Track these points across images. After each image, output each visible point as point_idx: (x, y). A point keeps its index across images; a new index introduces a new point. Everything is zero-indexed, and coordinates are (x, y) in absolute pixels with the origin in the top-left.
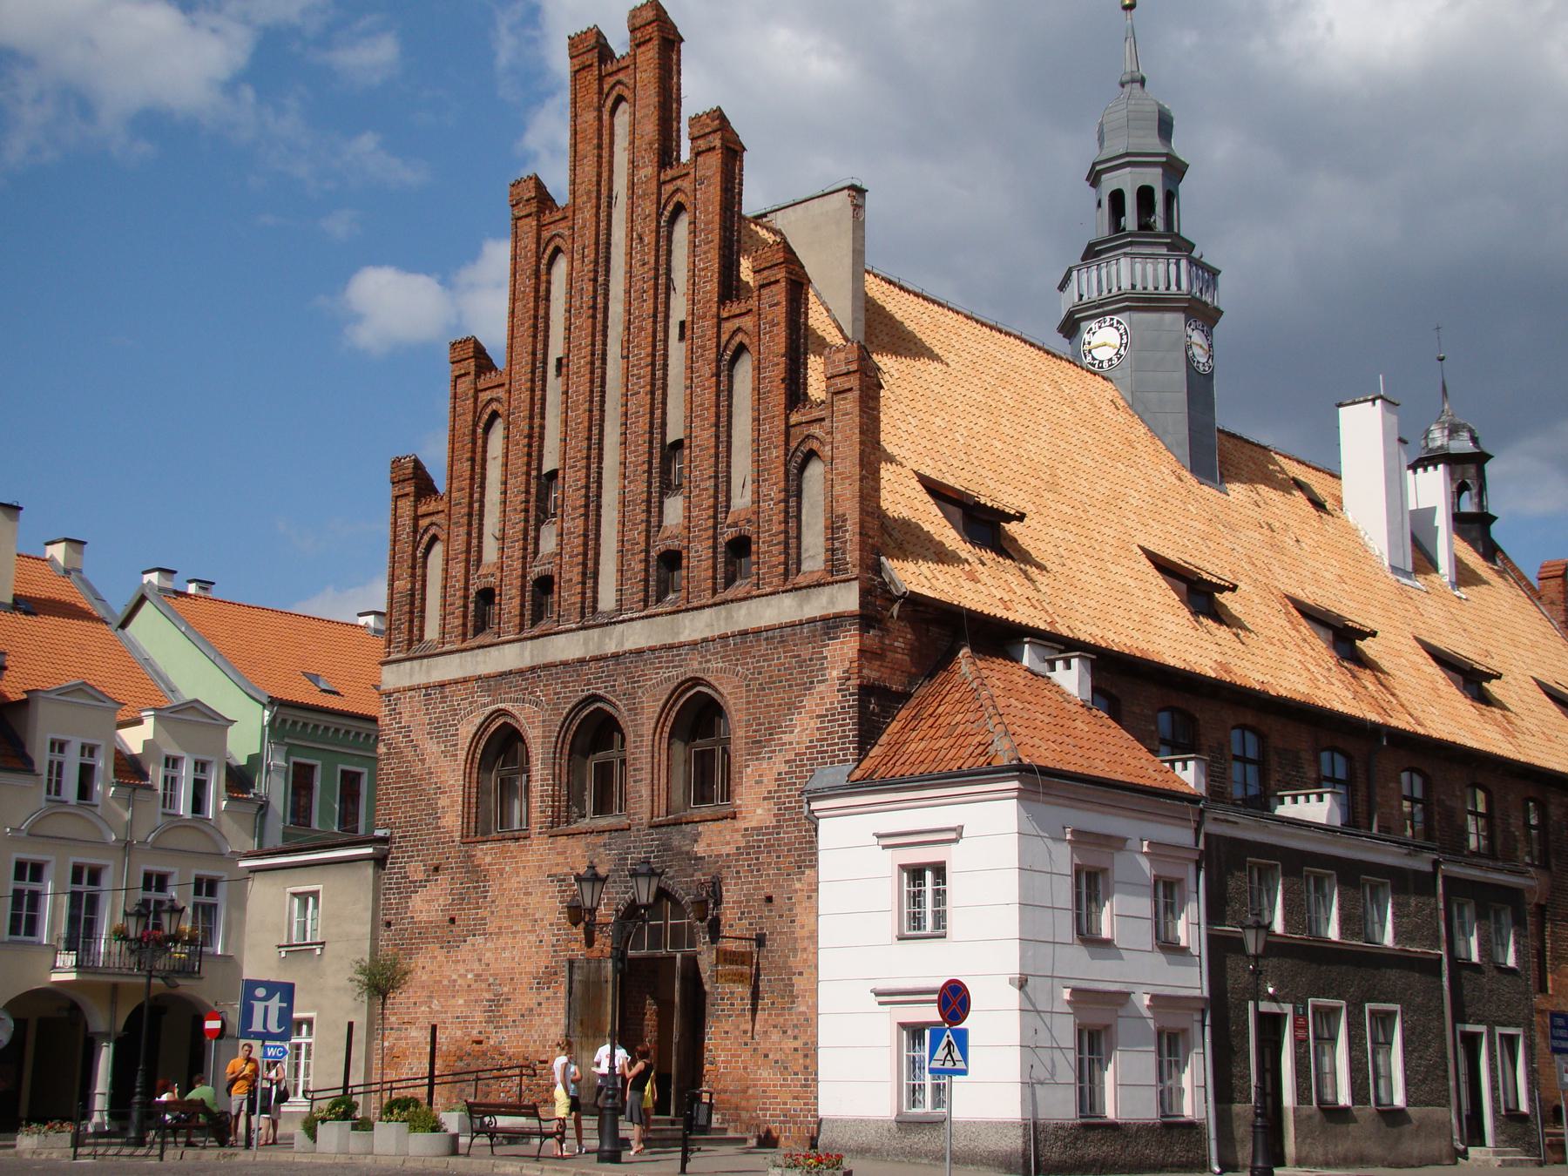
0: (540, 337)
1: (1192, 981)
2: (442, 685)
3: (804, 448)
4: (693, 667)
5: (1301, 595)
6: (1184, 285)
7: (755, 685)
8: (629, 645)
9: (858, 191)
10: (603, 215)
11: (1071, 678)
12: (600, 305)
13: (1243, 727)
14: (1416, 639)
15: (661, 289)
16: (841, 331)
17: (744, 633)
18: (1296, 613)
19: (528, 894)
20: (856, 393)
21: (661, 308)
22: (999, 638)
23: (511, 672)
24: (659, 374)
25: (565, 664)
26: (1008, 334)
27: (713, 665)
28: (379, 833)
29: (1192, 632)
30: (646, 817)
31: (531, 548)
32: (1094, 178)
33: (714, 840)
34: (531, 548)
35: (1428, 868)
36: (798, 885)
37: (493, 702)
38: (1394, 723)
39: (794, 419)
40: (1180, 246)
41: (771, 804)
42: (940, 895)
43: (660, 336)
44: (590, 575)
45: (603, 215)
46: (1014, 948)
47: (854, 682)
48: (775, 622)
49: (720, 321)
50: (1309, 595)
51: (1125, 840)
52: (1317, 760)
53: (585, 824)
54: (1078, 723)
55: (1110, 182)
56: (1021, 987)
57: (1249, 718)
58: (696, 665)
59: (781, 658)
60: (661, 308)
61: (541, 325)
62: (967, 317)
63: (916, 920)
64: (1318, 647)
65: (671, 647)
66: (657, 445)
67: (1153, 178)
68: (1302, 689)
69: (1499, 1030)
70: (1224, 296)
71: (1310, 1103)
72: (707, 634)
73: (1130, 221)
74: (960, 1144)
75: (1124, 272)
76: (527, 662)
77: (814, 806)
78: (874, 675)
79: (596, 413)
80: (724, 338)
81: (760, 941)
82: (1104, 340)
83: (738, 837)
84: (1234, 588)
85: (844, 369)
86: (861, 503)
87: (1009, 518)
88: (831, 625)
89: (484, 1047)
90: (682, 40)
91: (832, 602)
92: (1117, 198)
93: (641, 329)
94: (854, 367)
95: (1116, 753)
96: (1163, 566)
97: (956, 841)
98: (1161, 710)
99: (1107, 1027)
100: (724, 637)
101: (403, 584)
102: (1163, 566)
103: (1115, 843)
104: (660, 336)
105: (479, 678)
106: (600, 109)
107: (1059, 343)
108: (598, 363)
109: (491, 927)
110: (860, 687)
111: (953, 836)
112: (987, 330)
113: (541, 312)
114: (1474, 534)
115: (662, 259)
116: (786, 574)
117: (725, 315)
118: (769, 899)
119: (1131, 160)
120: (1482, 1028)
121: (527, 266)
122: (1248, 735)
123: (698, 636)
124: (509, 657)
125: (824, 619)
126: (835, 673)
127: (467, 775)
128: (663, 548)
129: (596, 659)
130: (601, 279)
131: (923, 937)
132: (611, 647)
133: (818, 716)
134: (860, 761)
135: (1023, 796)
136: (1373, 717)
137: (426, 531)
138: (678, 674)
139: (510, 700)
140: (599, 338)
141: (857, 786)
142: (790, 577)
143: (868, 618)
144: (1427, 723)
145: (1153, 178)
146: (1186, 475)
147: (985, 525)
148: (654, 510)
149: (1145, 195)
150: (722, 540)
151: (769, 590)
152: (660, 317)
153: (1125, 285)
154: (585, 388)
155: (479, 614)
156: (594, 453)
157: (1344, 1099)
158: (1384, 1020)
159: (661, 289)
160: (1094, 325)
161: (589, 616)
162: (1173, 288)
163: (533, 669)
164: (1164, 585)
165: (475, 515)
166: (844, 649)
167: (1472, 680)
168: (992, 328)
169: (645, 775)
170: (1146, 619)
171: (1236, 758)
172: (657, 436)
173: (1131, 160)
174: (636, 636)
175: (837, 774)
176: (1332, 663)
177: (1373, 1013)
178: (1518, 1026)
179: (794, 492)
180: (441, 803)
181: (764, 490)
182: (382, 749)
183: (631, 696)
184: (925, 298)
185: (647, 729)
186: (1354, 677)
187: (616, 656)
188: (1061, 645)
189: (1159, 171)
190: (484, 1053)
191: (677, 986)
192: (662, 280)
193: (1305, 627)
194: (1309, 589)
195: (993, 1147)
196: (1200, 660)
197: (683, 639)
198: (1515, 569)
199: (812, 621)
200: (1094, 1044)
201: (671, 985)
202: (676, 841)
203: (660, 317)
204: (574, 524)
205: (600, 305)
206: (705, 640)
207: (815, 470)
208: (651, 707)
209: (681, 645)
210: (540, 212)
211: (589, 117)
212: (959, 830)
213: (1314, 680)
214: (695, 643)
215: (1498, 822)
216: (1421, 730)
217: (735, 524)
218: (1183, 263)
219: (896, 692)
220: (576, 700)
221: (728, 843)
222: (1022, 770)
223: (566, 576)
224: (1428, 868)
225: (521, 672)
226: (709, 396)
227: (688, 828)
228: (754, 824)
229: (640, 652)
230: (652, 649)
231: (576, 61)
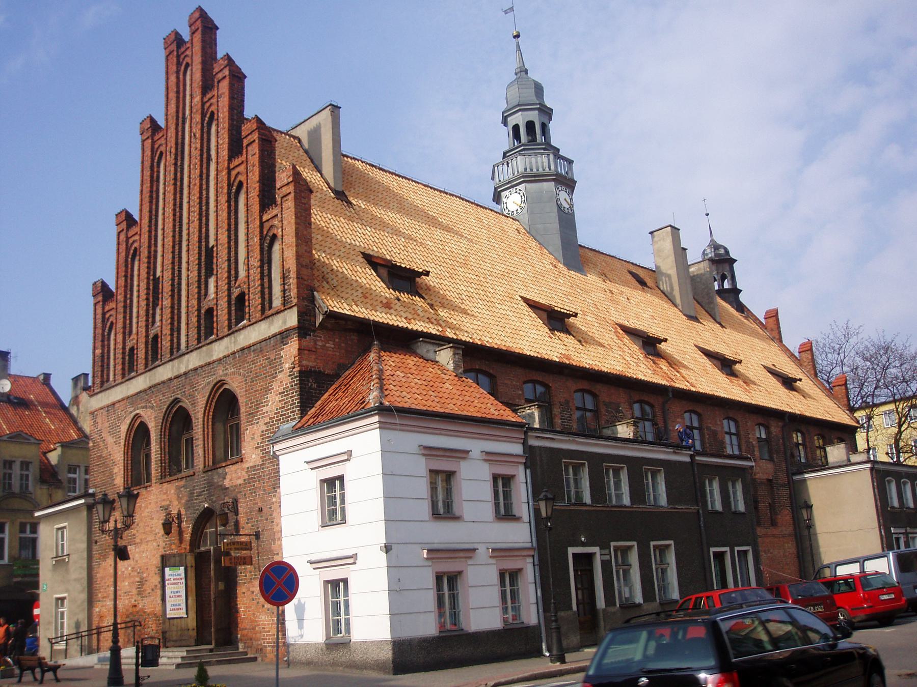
0: (154, 201)
1: (520, 534)
2: (114, 404)
3: (271, 234)
4: (220, 373)
5: (626, 323)
6: (553, 168)
7: (249, 380)
8: (191, 367)
9: (335, 109)
10: (180, 128)
11: (446, 357)
12: (179, 177)
13: (583, 391)
14: (696, 346)
15: (205, 160)
16: (328, 184)
17: (243, 349)
18: (621, 332)
19: (152, 519)
20: (292, 195)
21: (205, 171)
22: (402, 341)
23: (141, 392)
24: (204, 208)
25: (163, 382)
26: (453, 195)
27: (229, 371)
28: (91, 491)
29: (549, 340)
30: (202, 466)
31: (150, 320)
32: (505, 122)
33: (234, 476)
34: (150, 320)
35: (688, 459)
36: (274, 500)
37: (135, 410)
38: (677, 385)
39: (265, 218)
40: (549, 147)
41: (258, 451)
42: (497, 505)
43: (204, 187)
44: (175, 329)
45: (180, 128)
46: (381, 527)
47: (297, 369)
48: (257, 340)
49: (229, 171)
50: (632, 323)
51: (467, 452)
52: (631, 408)
53: (180, 476)
54: (447, 385)
55: (512, 121)
56: (387, 552)
57: (585, 385)
58: (221, 373)
59: (261, 361)
60: (205, 171)
61: (154, 196)
62: (425, 186)
63: (333, 513)
64: (634, 349)
65: (209, 364)
66: (203, 249)
67: (534, 116)
68: (618, 368)
69: (737, 549)
70: (577, 173)
71: (615, 605)
72: (226, 353)
73: (524, 137)
74: (358, 657)
75: (520, 163)
76: (148, 384)
77: (277, 447)
78: (311, 364)
79: (177, 237)
80: (232, 179)
81: (257, 535)
82: (513, 201)
83: (244, 473)
84: (576, 315)
85: (286, 182)
86: (297, 259)
87: (419, 274)
88: (283, 336)
89: (137, 609)
90: (217, 28)
91: (285, 322)
92: (516, 128)
93: (195, 185)
94: (291, 179)
95: (478, 400)
96: (534, 306)
97: (348, 460)
98: (525, 382)
99: (460, 573)
100: (234, 353)
101: (98, 351)
102: (534, 306)
103: (463, 454)
104: (204, 187)
105: (128, 397)
106: (178, 72)
107: (493, 205)
108: (178, 210)
109: (138, 540)
110: (300, 372)
111: (346, 458)
112: (438, 193)
113: (155, 188)
114: (731, 299)
115: (205, 145)
116: (263, 310)
117: (232, 167)
118: (261, 510)
119: (521, 107)
120: (727, 549)
121: (148, 164)
122: (762, 428)
123: (221, 356)
124: (140, 383)
125: (280, 333)
126: (287, 366)
127: (126, 453)
128: (207, 307)
129: (177, 377)
130: (179, 163)
131: (342, 524)
132: (183, 370)
133: (280, 393)
134: (301, 418)
135: (383, 426)
136: (664, 382)
137: (108, 319)
138: (213, 379)
139: (143, 407)
140: (178, 196)
141: (299, 431)
142: (266, 312)
143: (304, 329)
144: (698, 386)
145: (534, 116)
146: (561, 266)
147: (403, 279)
148: (203, 286)
149: (530, 125)
150: (233, 297)
151: (254, 320)
152: (204, 176)
153: (521, 170)
154: (171, 225)
155: (129, 369)
156: (177, 259)
157: (639, 599)
158: (663, 550)
159: (205, 160)
160: (507, 193)
161: (176, 353)
162: (547, 169)
163: (150, 388)
164: (534, 315)
165: (128, 307)
166: (291, 349)
167: (726, 365)
168: (441, 192)
169: (200, 442)
170: (516, 331)
171: (726, 433)
172: (204, 244)
173: (521, 107)
174: (193, 360)
175: (287, 427)
176: (641, 357)
177: (655, 547)
178: (748, 545)
179: (266, 261)
180: (115, 471)
181: (251, 263)
182: (91, 444)
183: (192, 396)
184: (396, 175)
185: (200, 415)
186: (654, 363)
187: (185, 374)
188: (440, 341)
189: (537, 112)
190: (137, 612)
191: (212, 566)
192: (205, 156)
193: (626, 339)
194: (631, 321)
195: (376, 658)
196: (552, 353)
197: (215, 358)
198: (753, 315)
199: (275, 336)
200: (448, 584)
201: (228, 567)
202: (216, 479)
203: (204, 176)
204: (167, 302)
205: (179, 177)
206: (225, 357)
207: (277, 247)
208: (201, 401)
209: (214, 362)
210: (153, 135)
211: (173, 78)
212: (349, 453)
213: (628, 364)
214: (220, 360)
215: (742, 436)
216: (693, 389)
217: (239, 286)
218: (551, 156)
219: (328, 375)
220: (168, 403)
221: (239, 478)
222: (382, 410)
223: (164, 333)
224: (688, 459)
225: (145, 391)
226: (225, 214)
227: (220, 471)
228: (251, 464)
229: (196, 369)
230: (201, 367)
231: (168, 50)
